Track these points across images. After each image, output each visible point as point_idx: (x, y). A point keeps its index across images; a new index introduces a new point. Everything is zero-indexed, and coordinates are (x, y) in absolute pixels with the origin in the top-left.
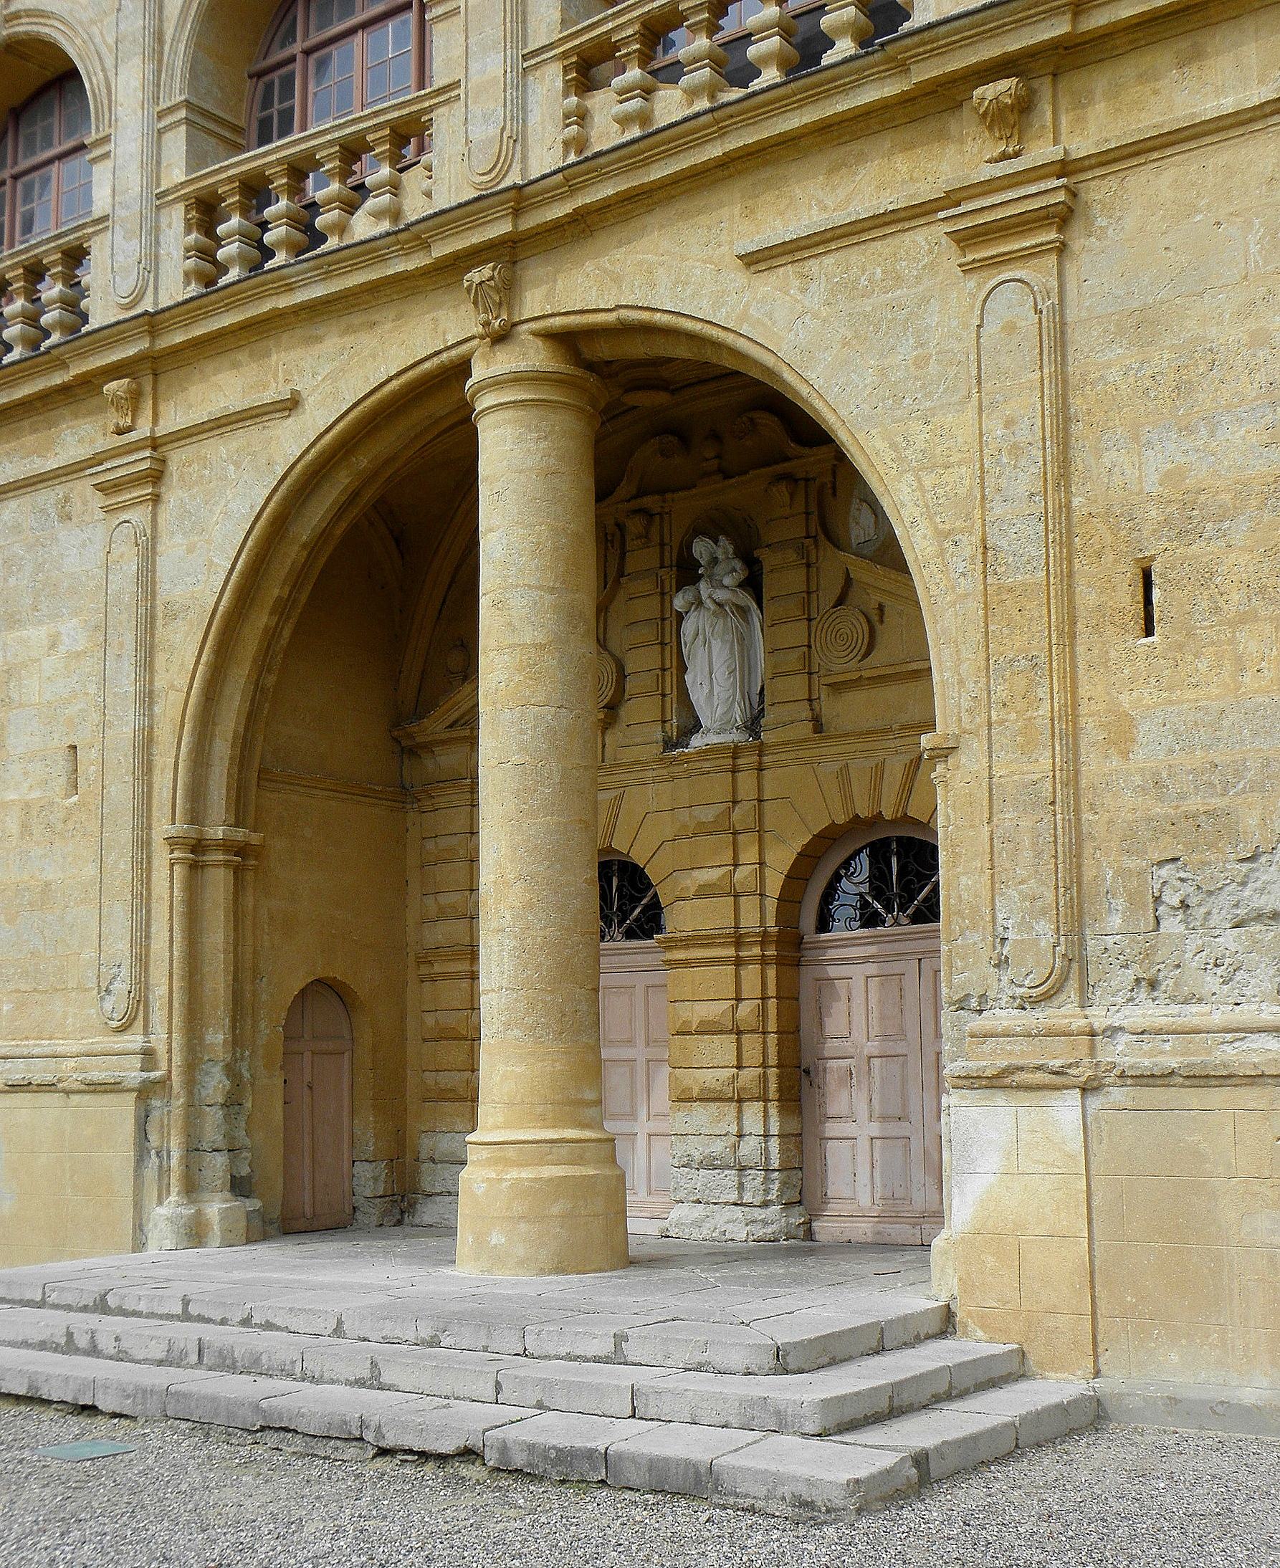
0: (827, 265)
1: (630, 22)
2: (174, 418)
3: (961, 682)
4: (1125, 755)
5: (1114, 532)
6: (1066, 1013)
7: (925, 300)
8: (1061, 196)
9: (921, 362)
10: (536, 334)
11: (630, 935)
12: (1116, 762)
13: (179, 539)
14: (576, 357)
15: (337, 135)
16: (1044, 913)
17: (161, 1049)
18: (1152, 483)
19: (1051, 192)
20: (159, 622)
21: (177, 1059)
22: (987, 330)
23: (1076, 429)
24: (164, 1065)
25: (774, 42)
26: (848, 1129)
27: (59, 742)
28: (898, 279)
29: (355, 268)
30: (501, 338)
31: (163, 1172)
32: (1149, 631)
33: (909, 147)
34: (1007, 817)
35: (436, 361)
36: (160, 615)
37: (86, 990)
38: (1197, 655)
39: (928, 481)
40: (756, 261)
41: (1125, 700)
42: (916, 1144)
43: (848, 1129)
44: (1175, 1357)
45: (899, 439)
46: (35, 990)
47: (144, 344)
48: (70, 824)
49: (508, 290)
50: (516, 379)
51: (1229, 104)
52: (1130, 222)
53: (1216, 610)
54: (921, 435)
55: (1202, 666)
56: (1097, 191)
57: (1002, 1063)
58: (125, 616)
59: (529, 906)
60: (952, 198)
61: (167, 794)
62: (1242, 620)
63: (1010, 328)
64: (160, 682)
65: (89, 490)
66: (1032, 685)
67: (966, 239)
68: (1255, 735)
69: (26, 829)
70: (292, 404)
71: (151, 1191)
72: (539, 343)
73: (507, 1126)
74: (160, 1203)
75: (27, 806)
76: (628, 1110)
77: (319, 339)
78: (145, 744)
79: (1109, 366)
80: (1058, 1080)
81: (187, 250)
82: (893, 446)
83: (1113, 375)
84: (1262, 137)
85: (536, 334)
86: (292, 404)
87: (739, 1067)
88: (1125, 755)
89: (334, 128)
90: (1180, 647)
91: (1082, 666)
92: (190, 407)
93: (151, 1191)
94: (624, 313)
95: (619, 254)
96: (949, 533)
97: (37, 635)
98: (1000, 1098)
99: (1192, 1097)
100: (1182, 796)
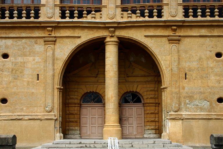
0: (154, 39)
1: (130, 7)
2: (58, 35)
3: (168, 82)
4: (184, 90)
5: (183, 70)
6: (179, 113)
7: (165, 44)
8: (55, 40)
9: (164, 51)
10: (117, 37)
11: (134, 103)
12: (183, 90)
13: (58, 50)
14: (119, 40)
15: (87, 6)
16: (177, 104)
17: (56, 114)
18: (187, 66)
19: (177, 38)
20: (55, 60)
21: (58, 116)
22: (172, 49)
23: (180, 60)
24: (57, 116)
25: (69, 15)
26: (126, 125)
27: (36, 73)
28: (162, 42)
29: (93, 24)
30: (112, 36)
31: (57, 130)
32: (186, 79)
33: (163, 29)
34: (173, 95)
35: (102, 37)
36: (55, 59)
37: (41, 107)
38: (191, 82)
39: (165, 62)
40: (145, 36)
41: (184, 85)
42: (134, 127)
43: (126, 125)
44: (190, 143)
45: (162, 57)
46: (31, 106)
47: (56, 25)
48: (38, 85)
49: (114, 32)
50: (115, 41)
51: (195, 34)
52: (185, 42)
53: (192, 78)
54: (164, 57)
55: (191, 83)
56: (58, 40)
57: (175, 117)
58: (50, 59)
59: (115, 100)
60: (169, 36)
61: (57, 82)
62: (194, 79)
63: (174, 50)
64: (55, 68)
65: (43, 41)
66: (176, 83)
67: (45, 41)
68: (196, 90)
69: (28, 84)
70: (79, 37)
71: (56, 132)
72: (116, 38)
73: (113, 123)
74: (57, 134)
75: (28, 82)
76: (95, 123)
77: (84, 30)
78: (54, 76)
79: (183, 55)
81: (60, 13)
82: (161, 58)
83: (183, 56)
84: (197, 38)
85: (117, 37)
86: (79, 37)
87: (155, 118)
88: (184, 90)
89: (96, 6)
90: (189, 81)
91: (180, 82)
92: (61, 33)
93: (56, 132)
94: (129, 37)
95: (129, 31)
96: (167, 67)
97: (31, 59)
98: (174, 120)
99: (192, 121)
100: (189, 94)
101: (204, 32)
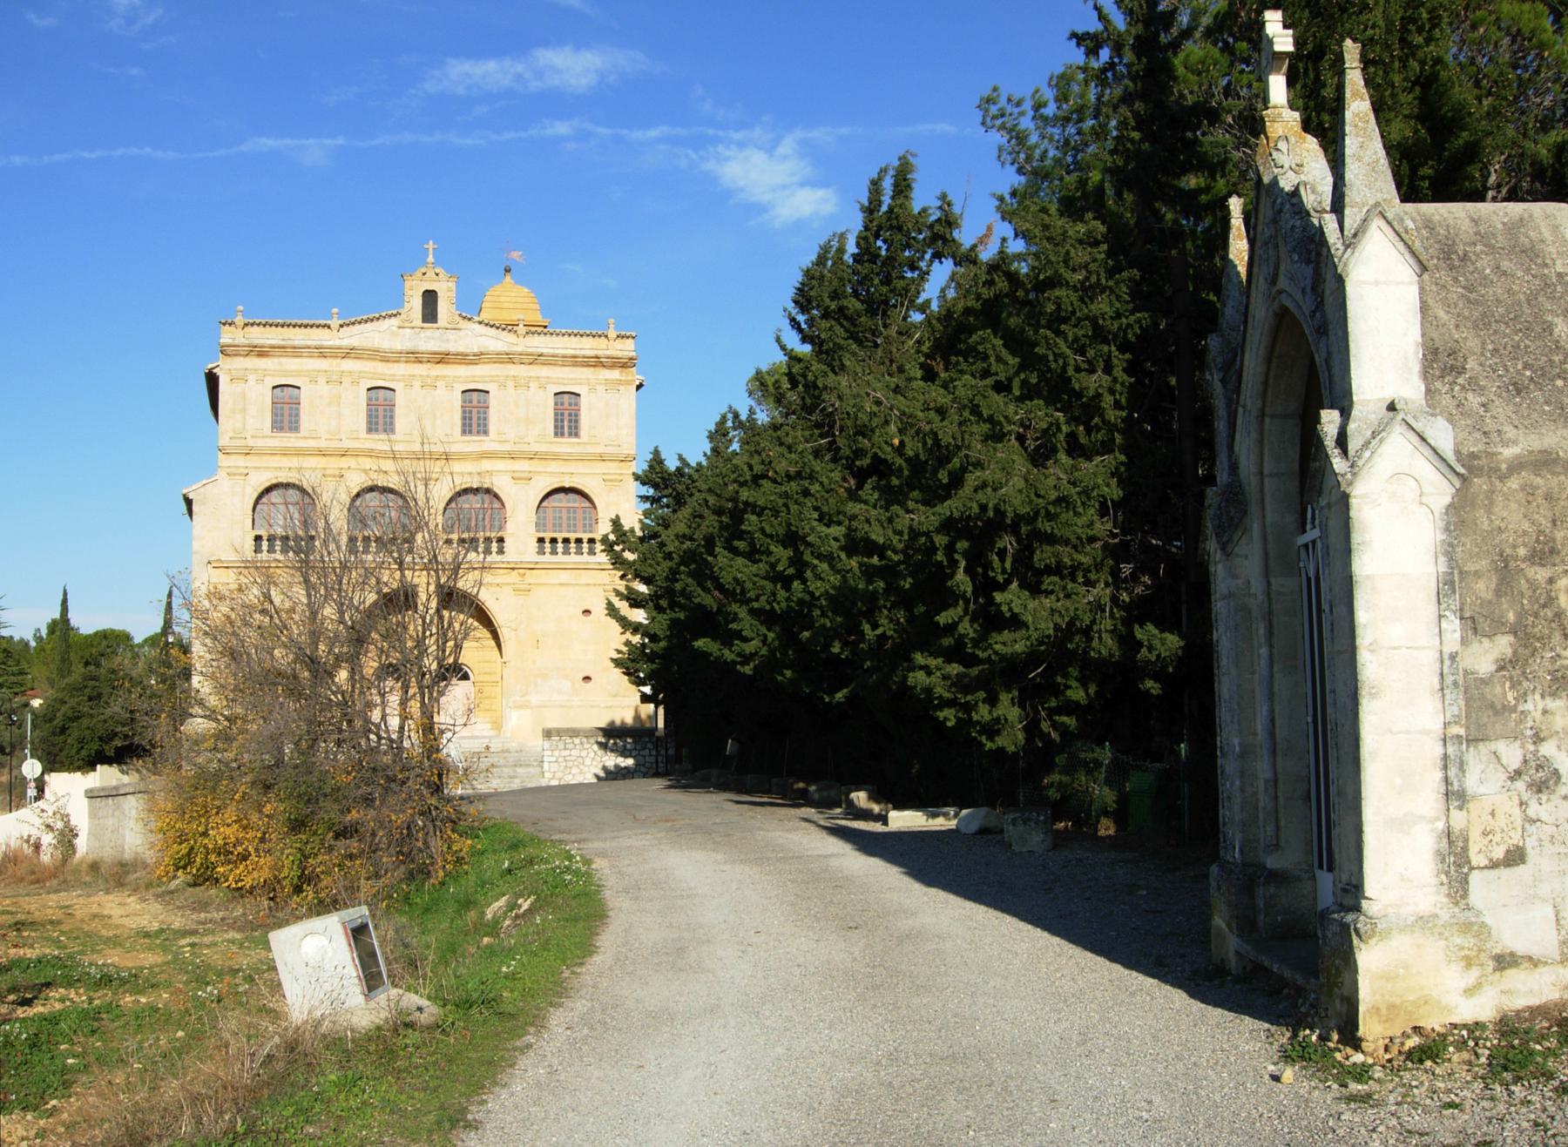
80: (527, 707)
101: (564, 576)
